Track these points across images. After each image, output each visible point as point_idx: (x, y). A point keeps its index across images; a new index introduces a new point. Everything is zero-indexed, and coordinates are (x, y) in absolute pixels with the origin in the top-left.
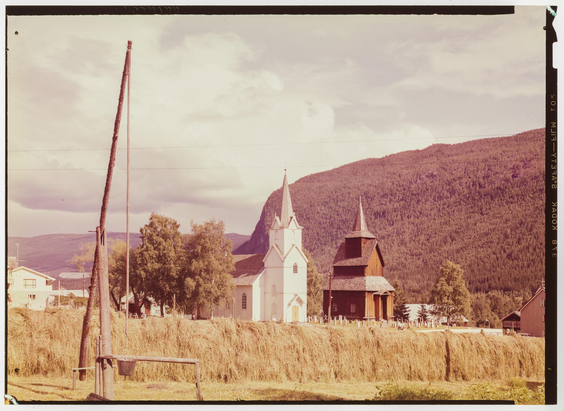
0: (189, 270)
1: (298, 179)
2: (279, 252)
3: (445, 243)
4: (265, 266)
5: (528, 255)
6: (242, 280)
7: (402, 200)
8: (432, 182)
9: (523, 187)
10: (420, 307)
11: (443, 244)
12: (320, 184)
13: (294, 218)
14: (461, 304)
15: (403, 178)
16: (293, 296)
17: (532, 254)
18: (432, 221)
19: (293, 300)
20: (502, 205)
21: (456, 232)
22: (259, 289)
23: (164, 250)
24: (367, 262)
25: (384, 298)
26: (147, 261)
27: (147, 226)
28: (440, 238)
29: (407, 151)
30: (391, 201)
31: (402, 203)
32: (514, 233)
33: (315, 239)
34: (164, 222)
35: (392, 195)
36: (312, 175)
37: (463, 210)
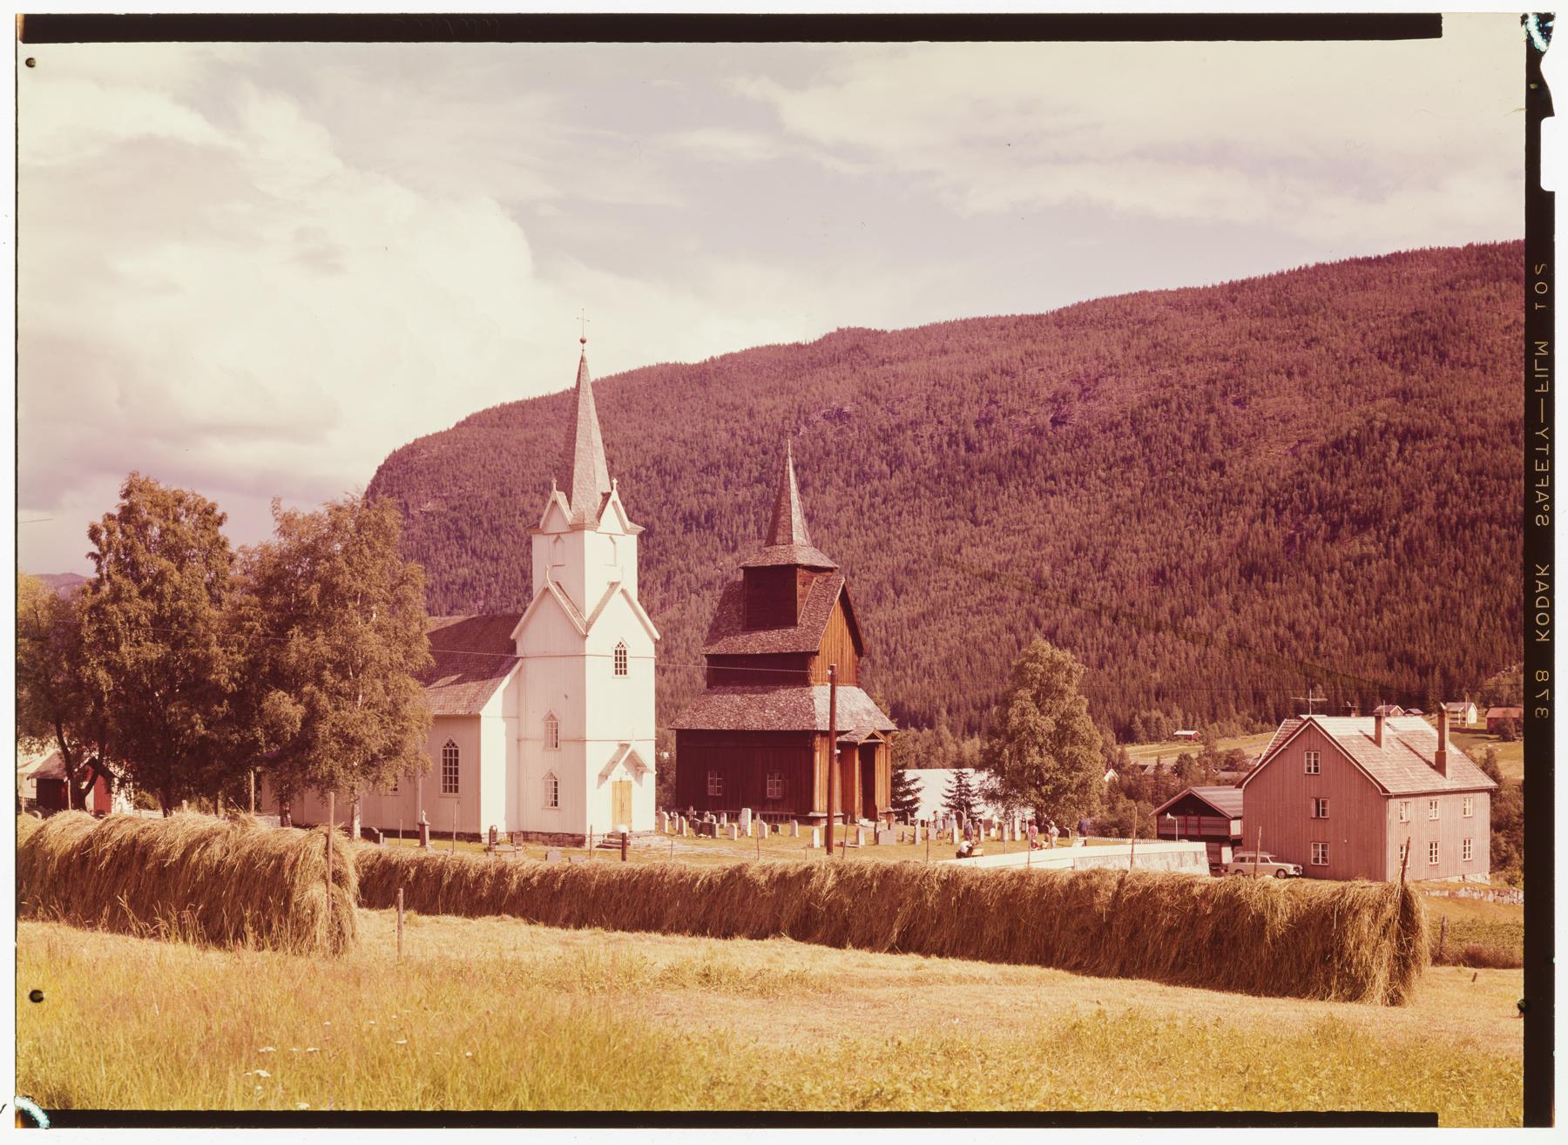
0: (275, 664)
1: (463, 418)
2: (567, 607)
3: (879, 601)
4: (520, 652)
5: (1099, 633)
6: (442, 698)
7: (759, 481)
8: (841, 432)
9: (1080, 452)
10: (953, 778)
11: (874, 605)
12: (530, 434)
13: (615, 496)
14: (1080, 770)
15: (759, 420)
16: (615, 747)
17: (1110, 633)
18: (841, 541)
19: (614, 763)
20: (1028, 499)
21: (908, 571)
22: (503, 726)
23: (176, 598)
24: (817, 640)
25: (868, 751)
26: (117, 635)
27: (110, 517)
28: (866, 587)
29: (769, 347)
30: (727, 483)
31: (759, 489)
32: (1059, 573)
33: (516, 587)
34: (170, 506)
35: (730, 466)
36: (503, 406)
37: (925, 510)
